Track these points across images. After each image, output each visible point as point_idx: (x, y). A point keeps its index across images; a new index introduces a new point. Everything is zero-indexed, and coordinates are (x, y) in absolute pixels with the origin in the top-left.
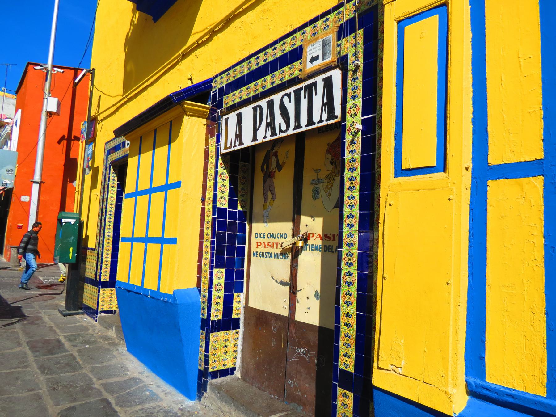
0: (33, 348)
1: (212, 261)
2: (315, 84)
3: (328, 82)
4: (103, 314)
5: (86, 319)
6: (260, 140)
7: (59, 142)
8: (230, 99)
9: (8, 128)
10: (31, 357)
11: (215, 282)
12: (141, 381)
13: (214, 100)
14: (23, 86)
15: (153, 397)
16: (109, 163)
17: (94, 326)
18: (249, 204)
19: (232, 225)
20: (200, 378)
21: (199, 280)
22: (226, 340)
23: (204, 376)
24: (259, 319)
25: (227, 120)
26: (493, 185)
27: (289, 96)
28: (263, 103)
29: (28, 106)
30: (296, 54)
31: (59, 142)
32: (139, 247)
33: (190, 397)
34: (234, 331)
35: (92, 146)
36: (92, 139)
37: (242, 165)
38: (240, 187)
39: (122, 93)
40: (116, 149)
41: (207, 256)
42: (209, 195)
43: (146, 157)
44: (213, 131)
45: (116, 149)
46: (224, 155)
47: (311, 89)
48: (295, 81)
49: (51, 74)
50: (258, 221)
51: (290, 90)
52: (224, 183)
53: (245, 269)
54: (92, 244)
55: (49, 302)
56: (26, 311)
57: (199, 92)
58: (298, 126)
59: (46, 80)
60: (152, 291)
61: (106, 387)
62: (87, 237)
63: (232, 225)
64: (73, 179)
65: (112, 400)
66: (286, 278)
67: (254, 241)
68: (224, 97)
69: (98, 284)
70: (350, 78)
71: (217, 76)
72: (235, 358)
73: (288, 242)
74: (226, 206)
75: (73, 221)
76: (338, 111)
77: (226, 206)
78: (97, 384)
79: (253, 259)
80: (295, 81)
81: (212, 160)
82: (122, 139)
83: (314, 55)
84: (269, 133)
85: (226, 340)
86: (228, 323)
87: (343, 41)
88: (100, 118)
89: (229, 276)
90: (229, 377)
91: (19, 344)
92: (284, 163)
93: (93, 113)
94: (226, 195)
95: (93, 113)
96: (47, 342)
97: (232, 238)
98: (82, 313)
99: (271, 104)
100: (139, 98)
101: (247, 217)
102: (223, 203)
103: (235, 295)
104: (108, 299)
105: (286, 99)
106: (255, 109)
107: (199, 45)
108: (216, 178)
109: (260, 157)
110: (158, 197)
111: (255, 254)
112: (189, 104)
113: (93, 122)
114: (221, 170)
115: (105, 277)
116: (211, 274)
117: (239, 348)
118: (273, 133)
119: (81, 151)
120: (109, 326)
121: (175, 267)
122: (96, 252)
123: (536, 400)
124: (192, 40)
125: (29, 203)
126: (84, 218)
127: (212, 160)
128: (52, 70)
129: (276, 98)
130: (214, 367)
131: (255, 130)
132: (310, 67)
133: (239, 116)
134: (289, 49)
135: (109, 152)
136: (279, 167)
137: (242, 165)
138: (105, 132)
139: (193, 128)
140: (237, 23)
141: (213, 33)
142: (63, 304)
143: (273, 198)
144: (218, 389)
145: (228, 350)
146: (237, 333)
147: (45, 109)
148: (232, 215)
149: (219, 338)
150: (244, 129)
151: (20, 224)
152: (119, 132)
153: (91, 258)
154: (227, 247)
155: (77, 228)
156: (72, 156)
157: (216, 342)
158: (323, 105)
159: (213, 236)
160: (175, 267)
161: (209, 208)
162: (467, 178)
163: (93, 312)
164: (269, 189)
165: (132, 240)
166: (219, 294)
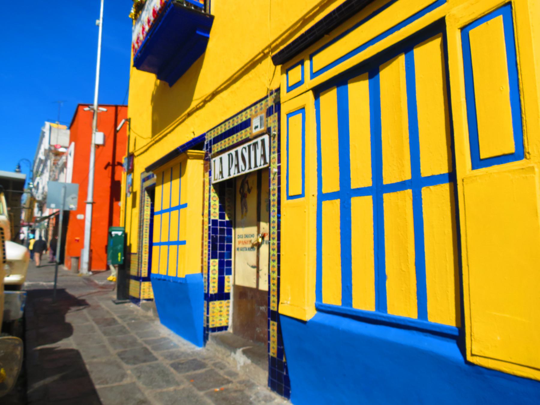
0: (97, 322)
1: (209, 255)
2: (257, 143)
3: (263, 141)
4: (144, 302)
5: (132, 306)
6: (232, 176)
7: (106, 168)
8: (216, 148)
9: (64, 158)
10: (96, 327)
11: (212, 268)
12: (168, 339)
13: (207, 148)
14: (75, 123)
15: (176, 346)
16: (144, 188)
17: (138, 310)
18: (233, 216)
19: (222, 231)
20: (204, 333)
21: (202, 268)
22: (221, 307)
23: (207, 329)
24: (243, 293)
25: (214, 161)
26: (386, 196)
27: (245, 148)
28: (233, 152)
29: (80, 138)
30: (247, 124)
31: (106, 168)
32: (164, 248)
33: (198, 344)
34: (227, 301)
35: (131, 176)
36: (131, 170)
37: (227, 191)
38: (227, 204)
39: (150, 136)
40: (148, 178)
41: (206, 252)
42: (206, 211)
43: (167, 186)
44: (208, 169)
45: (148, 178)
46: (215, 185)
47: (255, 144)
48: (247, 140)
49: (98, 113)
50: (239, 227)
51: (246, 145)
52: (216, 203)
53: (233, 259)
54: (134, 250)
55: (105, 296)
56: (89, 302)
57: (197, 143)
58: (250, 168)
59: (93, 118)
60: (173, 277)
61: (146, 342)
62: (130, 245)
63: (222, 231)
64: (118, 199)
65: (149, 347)
66: (254, 263)
67: (237, 240)
68: (212, 146)
69: (139, 279)
70: (272, 141)
71: (208, 132)
72: (228, 319)
73: (254, 240)
74: (217, 218)
75: (120, 233)
76: (268, 161)
77: (217, 218)
78: (140, 340)
79: (237, 252)
80: (247, 140)
81: (207, 188)
82: (151, 173)
83: (256, 125)
84: (236, 171)
85: (221, 307)
86: (222, 295)
87: (269, 118)
88: (136, 154)
89: (221, 264)
90: (223, 332)
91: (87, 320)
92: (252, 188)
93: (131, 150)
94: (217, 211)
95: (131, 150)
96: (106, 319)
97: (222, 239)
98: (129, 302)
99: (237, 152)
100: (162, 141)
101: (231, 224)
102: (215, 216)
103: (226, 277)
104: (146, 290)
105: (244, 150)
106: (229, 155)
107: (197, 109)
108: (209, 200)
109: (239, 184)
110: (175, 213)
111: (238, 249)
112: (191, 152)
113: (131, 157)
114: (213, 194)
115: (144, 274)
116: (209, 263)
117: (231, 313)
118: (239, 172)
119: (124, 178)
120: (147, 308)
121: (186, 259)
122: (137, 255)
123: (337, 308)
124: (194, 105)
125: (83, 221)
126: (127, 230)
127: (207, 188)
128: (98, 109)
129: (239, 149)
130: (213, 325)
131: (229, 169)
132: (255, 132)
133: (221, 159)
134: (244, 119)
135: (144, 180)
136: (249, 191)
137: (227, 191)
138: (141, 164)
139: (194, 166)
140: (218, 97)
141: (205, 102)
142: (115, 297)
143: (246, 211)
144: (215, 338)
145: (222, 314)
146: (229, 302)
147: (93, 142)
148: (222, 224)
149: (215, 305)
150: (224, 168)
151: (77, 238)
152: (148, 169)
153: (134, 260)
154: (219, 244)
155: (123, 239)
156: (116, 178)
157: (214, 308)
158: (262, 156)
159: (209, 238)
160: (186, 259)
161: (206, 220)
162: (314, 200)
163: (136, 300)
164: (244, 205)
165: (160, 244)
166: (214, 276)
